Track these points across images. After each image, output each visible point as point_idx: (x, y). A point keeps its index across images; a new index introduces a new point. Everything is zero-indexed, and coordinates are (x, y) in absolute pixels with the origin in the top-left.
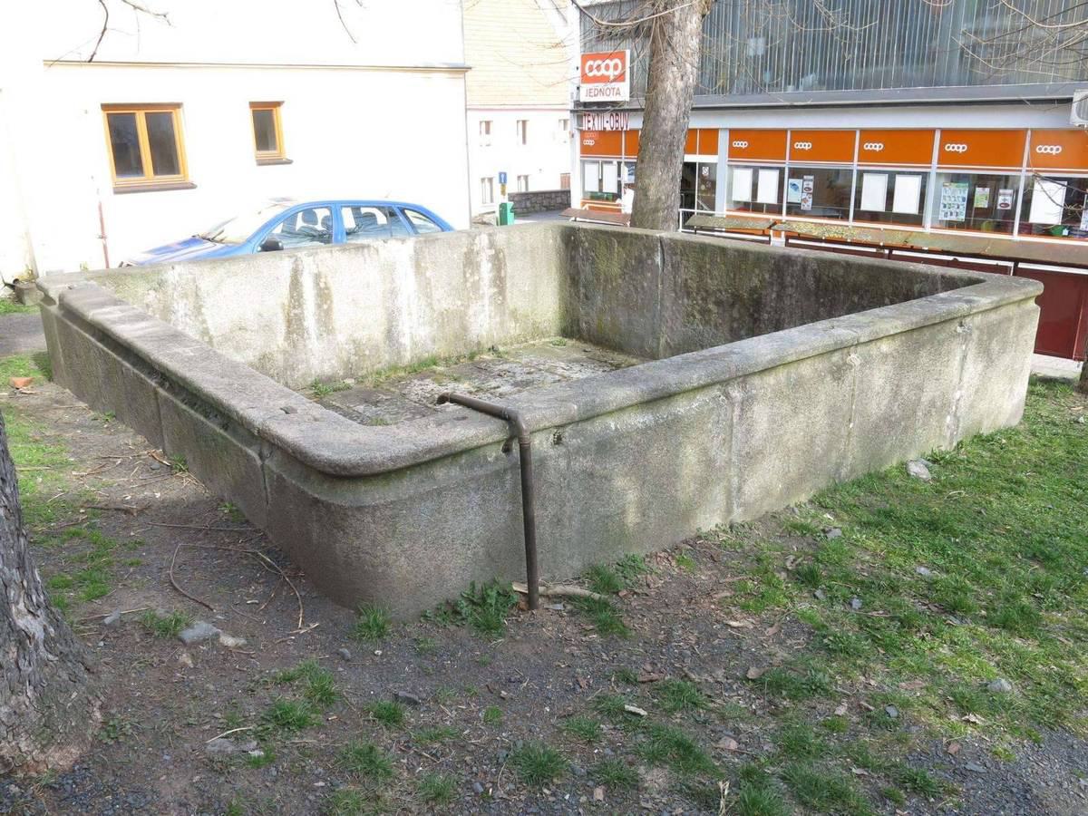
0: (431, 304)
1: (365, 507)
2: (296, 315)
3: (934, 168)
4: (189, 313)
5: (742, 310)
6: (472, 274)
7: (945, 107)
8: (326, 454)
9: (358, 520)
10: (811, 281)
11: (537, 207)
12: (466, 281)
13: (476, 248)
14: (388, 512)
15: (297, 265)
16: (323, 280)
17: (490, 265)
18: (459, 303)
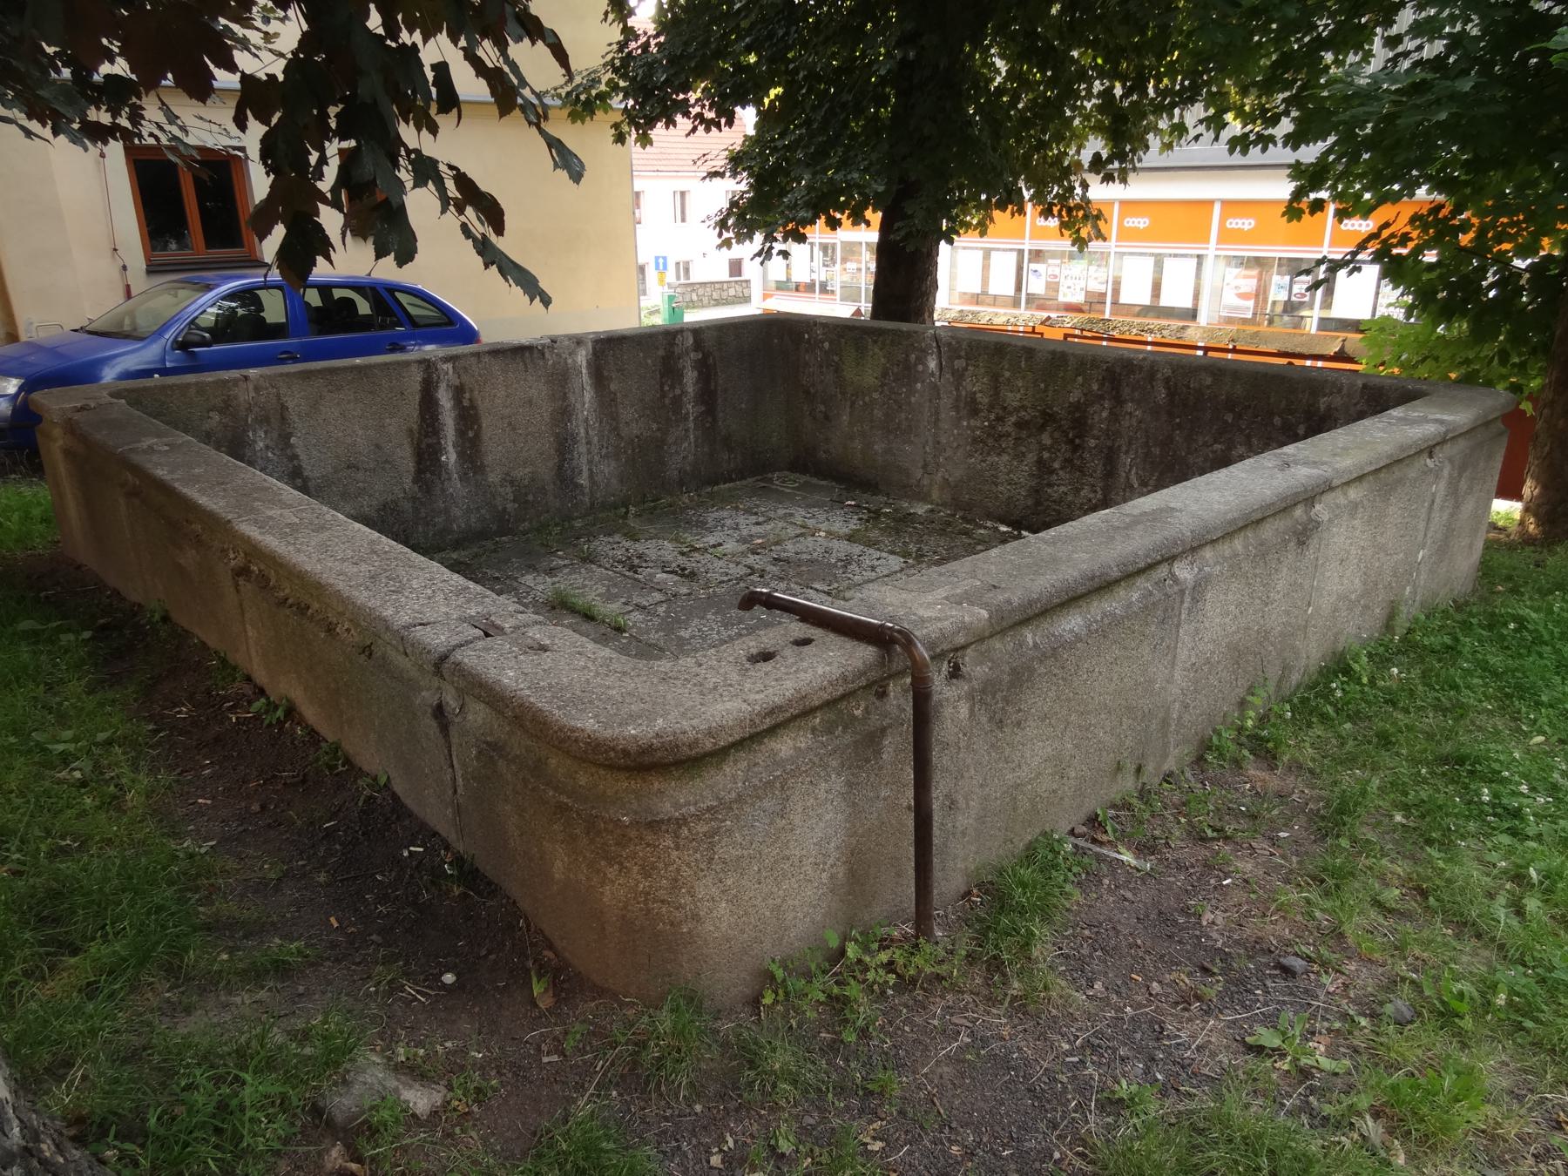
0: (616, 429)
1: (662, 821)
2: (429, 446)
3: (1211, 249)
4: (271, 444)
5: (1056, 435)
6: (672, 387)
7: (1200, 173)
8: (588, 723)
9: (648, 845)
10: (1162, 394)
11: (706, 300)
12: (663, 396)
13: (677, 350)
14: (702, 828)
15: (430, 376)
16: (467, 395)
17: (695, 374)
18: (655, 426)
